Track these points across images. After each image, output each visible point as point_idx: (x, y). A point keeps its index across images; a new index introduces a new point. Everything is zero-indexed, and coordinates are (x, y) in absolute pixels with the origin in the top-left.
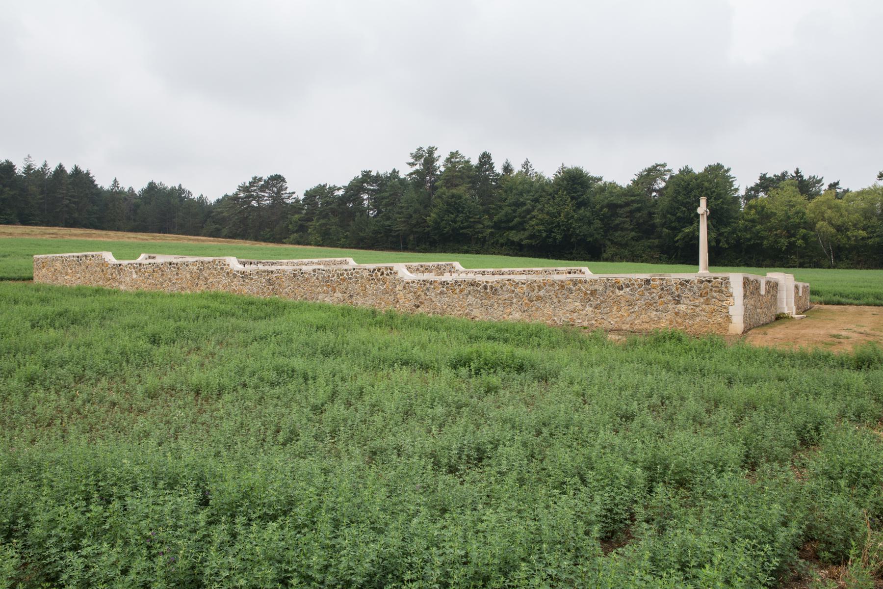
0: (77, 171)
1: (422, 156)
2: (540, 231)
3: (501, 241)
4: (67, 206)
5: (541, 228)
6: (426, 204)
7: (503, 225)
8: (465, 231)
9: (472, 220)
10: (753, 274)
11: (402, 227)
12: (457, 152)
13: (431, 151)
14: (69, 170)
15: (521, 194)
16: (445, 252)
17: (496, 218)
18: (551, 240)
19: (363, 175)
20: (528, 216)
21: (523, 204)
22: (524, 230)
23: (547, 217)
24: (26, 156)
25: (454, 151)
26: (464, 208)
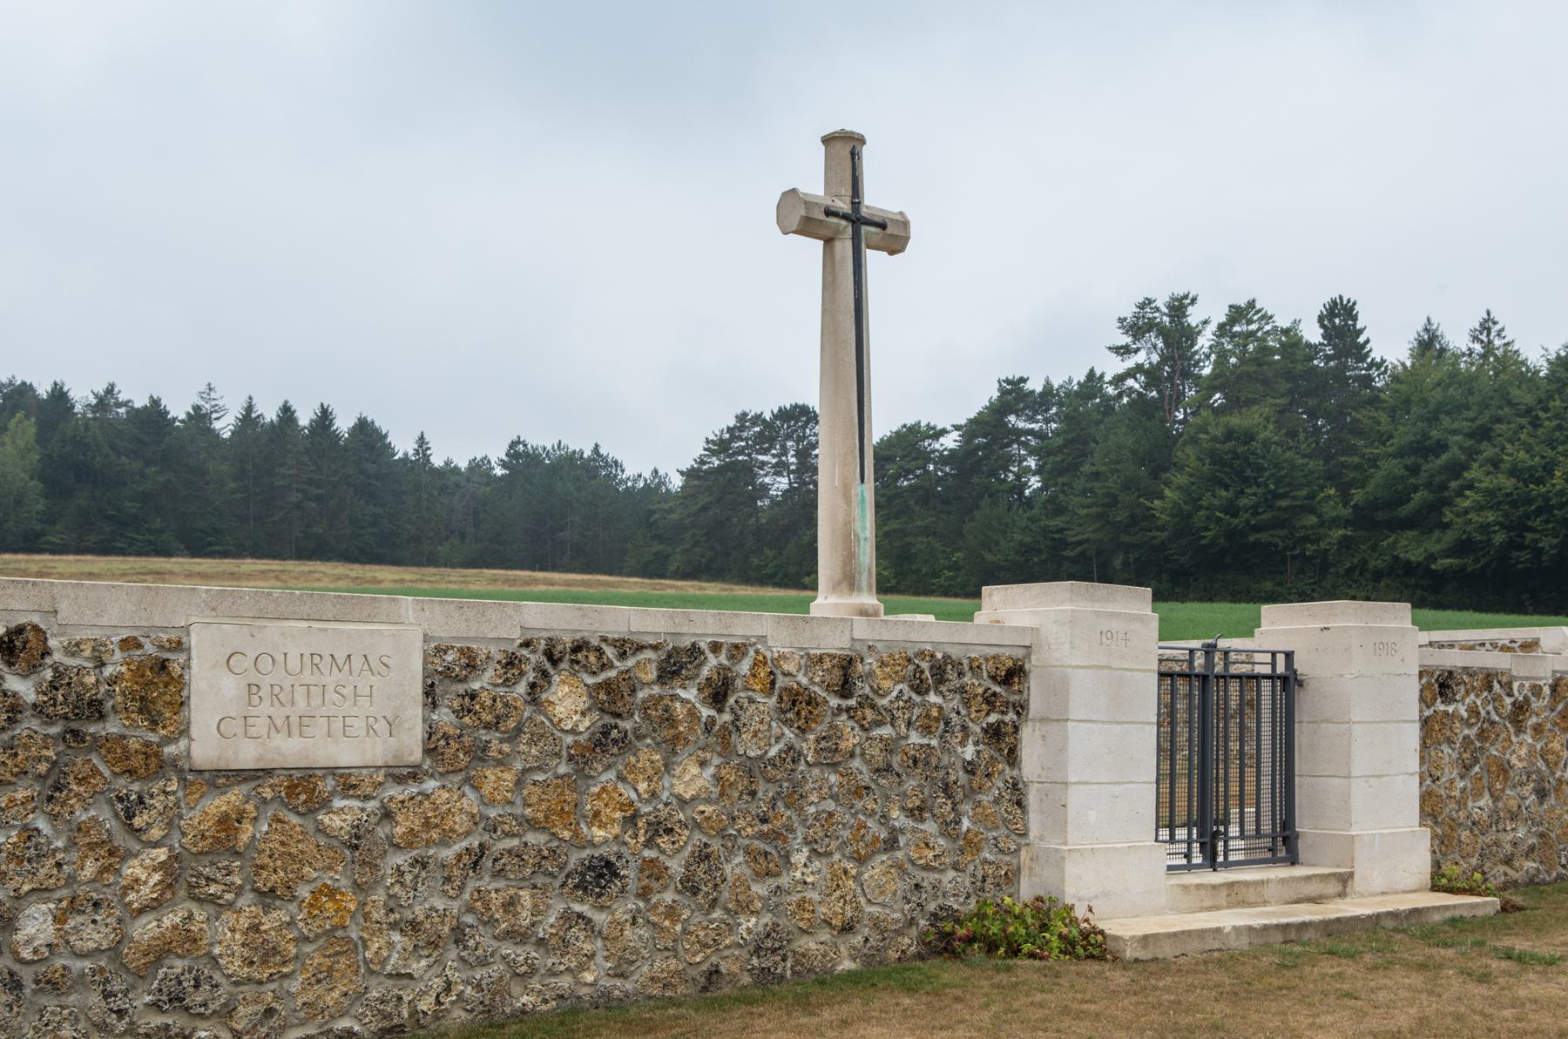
0: (364, 428)
1: (1151, 325)
2: (1484, 528)
3: (1375, 563)
4: (299, 506)
5: (1491, 517)
6: (1158, 459)
7: (1381, 515)
8: (1263, 537)
9: (1284, 503)
11: (1089, 532)
12: (1251, 304)
13: (1178, 307)
14: (343, 424)
15: (1433, 419)
17: (1358, 496)
18: (1525, 556)
19: (1003, 392)
21: (1442, 447)
22: (1446, 527)
23: (1509, 483)
24: (203, 388)
25: (1242, 303)
26: (1260, 469)
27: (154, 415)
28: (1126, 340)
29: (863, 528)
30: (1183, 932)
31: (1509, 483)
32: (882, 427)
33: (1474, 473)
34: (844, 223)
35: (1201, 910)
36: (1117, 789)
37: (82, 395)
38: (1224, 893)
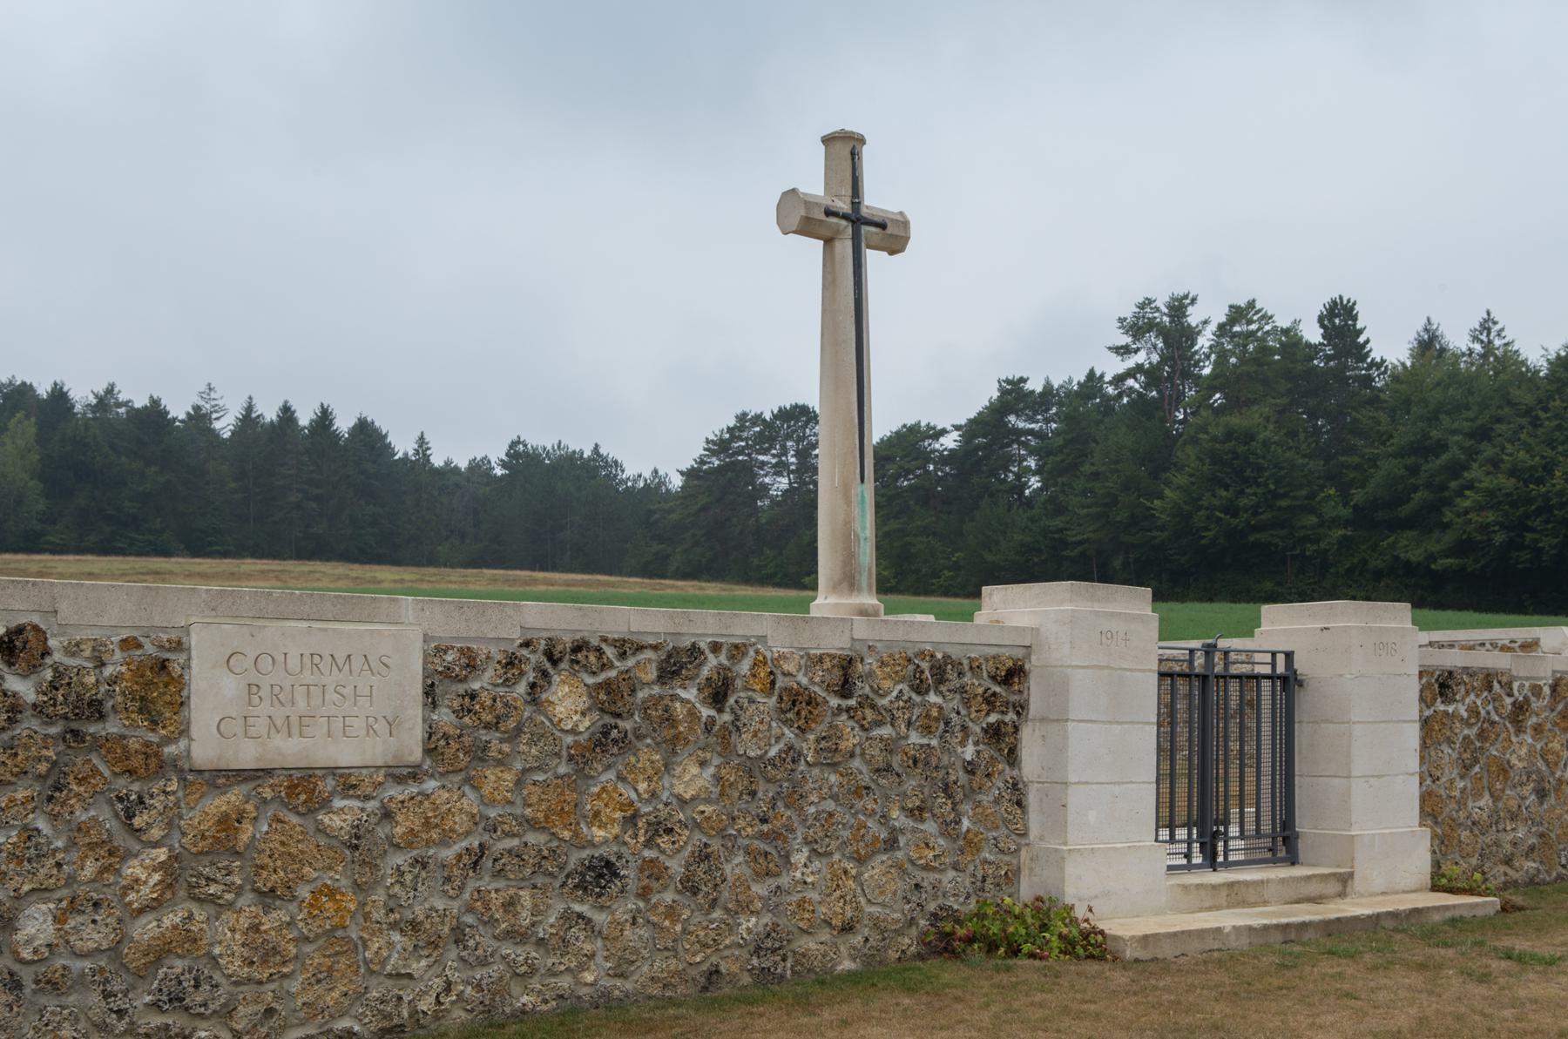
0: (364, 429)
2: (1484, 528)
3: (1376, 563)
5: (1491, 517)
8: (1263, 537)
9: (1284, 503)
10: (1478, 642)
12: (1251, 304)
13: (1178, 307)
14: (343, 424)
15: (1433, 419)
16: (1211, 600)
17: (1358, 496)
18: (1525, 556)
20: (1454, 484)
21: (1442, 447)
23: (1508, 483)
24: (203, 388)
25: (1242, 303)
26: (1260, 469)
27: (154, 415)
28: (1125, 340)
29: (864, 528)
30: (1183, 932)
31: (1508, 483)
32: (882, 427)
33: (1474, 473)
34: (844, 223)
35: (1201, 910)
36: (1117, 789)
37: (82, 394)
38: (1224, 893)
